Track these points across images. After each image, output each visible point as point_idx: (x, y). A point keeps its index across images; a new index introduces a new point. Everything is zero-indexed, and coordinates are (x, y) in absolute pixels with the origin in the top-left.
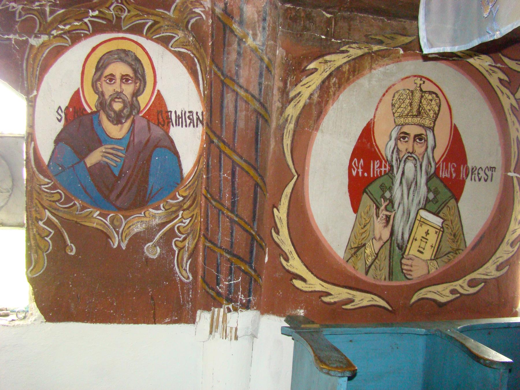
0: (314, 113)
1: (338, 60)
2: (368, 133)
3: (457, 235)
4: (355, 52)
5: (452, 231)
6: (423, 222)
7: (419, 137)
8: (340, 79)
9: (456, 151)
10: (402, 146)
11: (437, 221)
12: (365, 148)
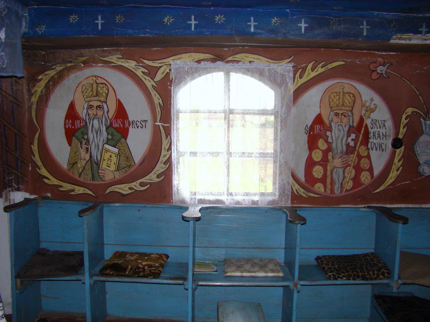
0: (44, 100)
1: (52, 73)
2: (72, 106)
3: (129, 157)
4: (59, 68)
5: (126, 155)
6: (107, 151)
7: (99, 107)
8: (54, 82)
9: (121, 112)
10: (91, 112)
11: (116, 150)
12: (72, 114)
